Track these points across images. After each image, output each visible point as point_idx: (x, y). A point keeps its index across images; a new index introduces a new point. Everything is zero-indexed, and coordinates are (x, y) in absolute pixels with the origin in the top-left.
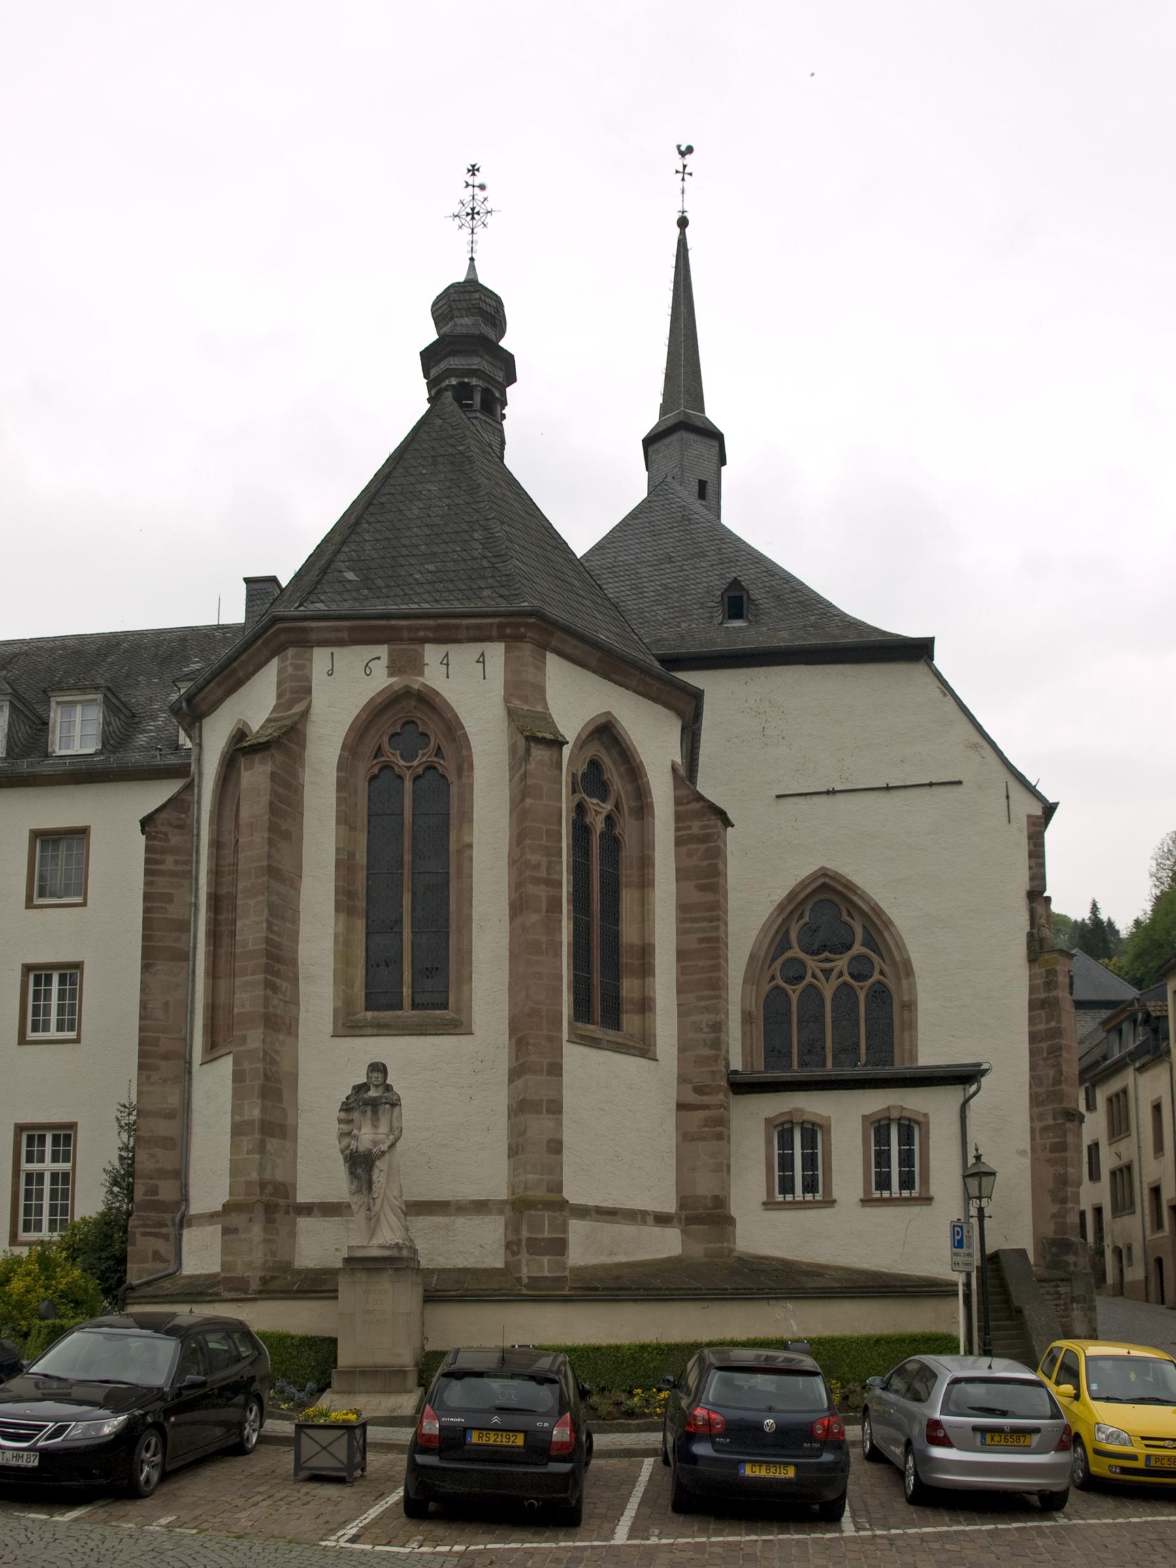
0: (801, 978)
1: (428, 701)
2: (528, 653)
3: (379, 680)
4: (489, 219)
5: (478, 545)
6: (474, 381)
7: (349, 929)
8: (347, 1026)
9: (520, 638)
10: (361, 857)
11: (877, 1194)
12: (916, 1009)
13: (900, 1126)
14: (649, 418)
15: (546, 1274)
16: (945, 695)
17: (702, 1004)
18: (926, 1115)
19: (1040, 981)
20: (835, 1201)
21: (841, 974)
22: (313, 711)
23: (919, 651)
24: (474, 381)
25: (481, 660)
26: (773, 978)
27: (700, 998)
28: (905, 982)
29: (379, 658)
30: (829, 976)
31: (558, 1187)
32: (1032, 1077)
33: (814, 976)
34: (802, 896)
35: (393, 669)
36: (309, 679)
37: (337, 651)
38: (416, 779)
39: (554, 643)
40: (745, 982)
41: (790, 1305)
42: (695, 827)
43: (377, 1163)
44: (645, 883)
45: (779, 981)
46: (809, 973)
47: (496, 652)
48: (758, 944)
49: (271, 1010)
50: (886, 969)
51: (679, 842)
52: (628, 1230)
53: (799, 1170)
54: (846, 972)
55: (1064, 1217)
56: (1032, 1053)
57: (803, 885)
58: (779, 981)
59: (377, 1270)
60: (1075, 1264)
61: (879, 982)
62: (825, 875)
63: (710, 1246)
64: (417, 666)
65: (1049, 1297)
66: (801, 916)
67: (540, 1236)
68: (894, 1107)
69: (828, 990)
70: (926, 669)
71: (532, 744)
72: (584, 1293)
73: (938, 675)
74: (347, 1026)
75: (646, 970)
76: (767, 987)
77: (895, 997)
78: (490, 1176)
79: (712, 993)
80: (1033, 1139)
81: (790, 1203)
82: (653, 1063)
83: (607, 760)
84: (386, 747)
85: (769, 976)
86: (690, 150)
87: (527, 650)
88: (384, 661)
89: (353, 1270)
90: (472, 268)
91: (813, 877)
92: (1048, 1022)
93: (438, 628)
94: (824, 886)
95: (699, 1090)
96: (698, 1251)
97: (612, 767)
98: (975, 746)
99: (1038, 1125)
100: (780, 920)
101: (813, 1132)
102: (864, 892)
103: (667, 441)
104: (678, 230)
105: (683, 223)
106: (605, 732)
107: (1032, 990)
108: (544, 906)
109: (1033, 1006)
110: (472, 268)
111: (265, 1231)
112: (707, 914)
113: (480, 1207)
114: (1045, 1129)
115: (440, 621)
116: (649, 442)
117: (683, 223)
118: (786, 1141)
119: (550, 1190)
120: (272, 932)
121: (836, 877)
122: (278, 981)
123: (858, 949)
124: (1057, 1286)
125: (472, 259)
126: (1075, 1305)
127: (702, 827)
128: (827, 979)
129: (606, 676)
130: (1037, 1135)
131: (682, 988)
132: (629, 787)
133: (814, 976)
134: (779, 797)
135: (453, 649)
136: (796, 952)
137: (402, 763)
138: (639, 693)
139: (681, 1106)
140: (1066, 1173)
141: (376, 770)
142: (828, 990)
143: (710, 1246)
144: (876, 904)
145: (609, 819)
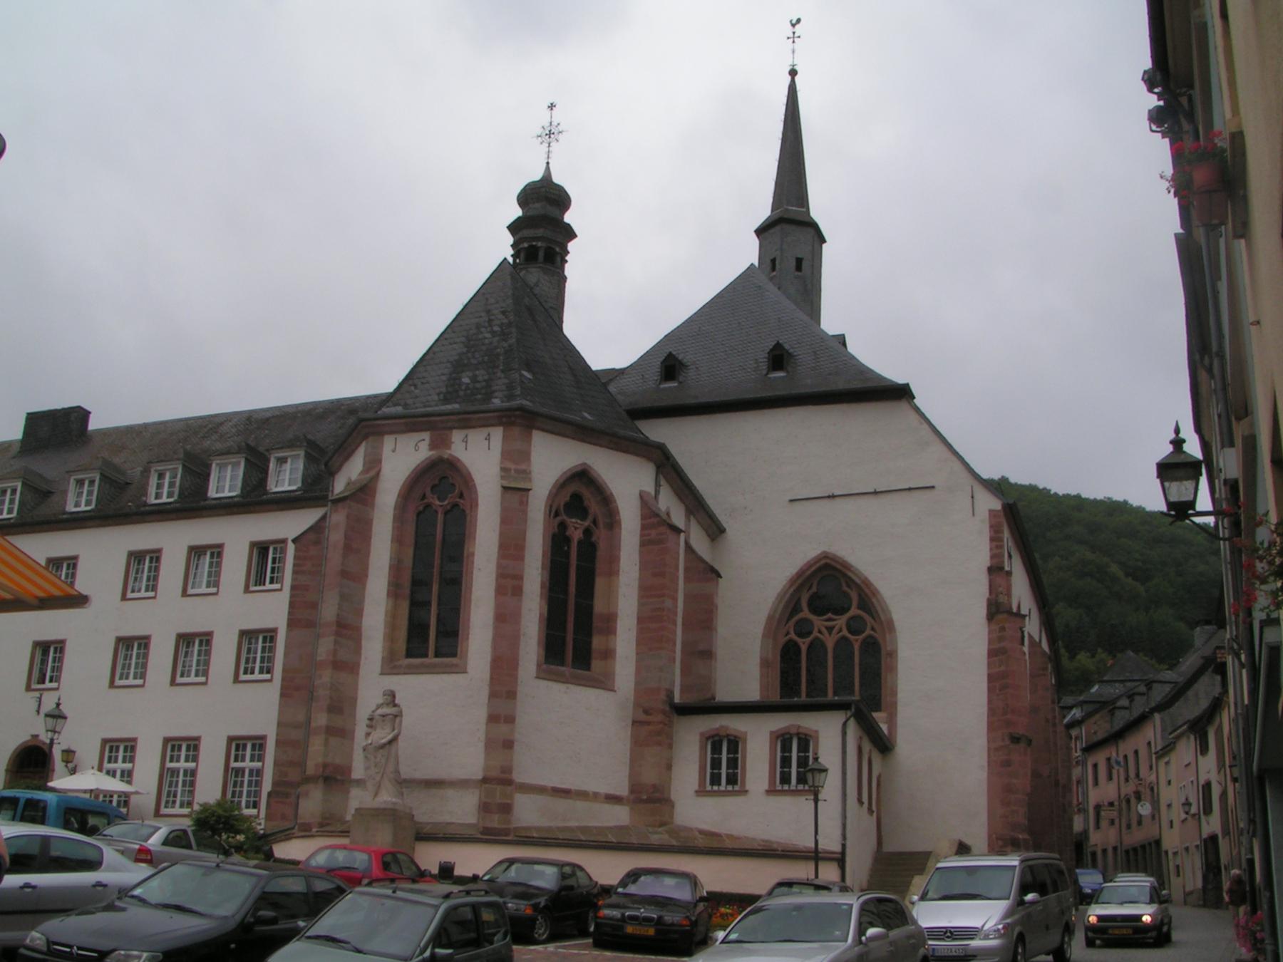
0: (810, 633)
6: (539, 244)
8: (390, 666)
11: (779, 788)
13: (799, 739)
14: (763, 211)
18: (816, 732)
21: (840, 630)
23: (901, 393)
25: (488, 438)
26: (788, 633)
30: (829, 630)
34: (809, 572)
35: (433, 446)
38: (446, 513)
44: (613, 572)
45: (793, 636)
46: (816, 630)
47: (497, 433)
50: (876, 626)
51: (643, 544)
52: (580, 805)
53: (724, 767)
57: (809, 565)
58: (793, 636)
61: (870, 636)
66: (811, 587)
69: (830, 642)
73: (917, 410)
74: (390, 666)
75: (610, 630)
76: (783, 640)
83: (586, 494)
84: (428, 493)
86: (799, 21)
87: (516, 431)
88: (427, 442)
91: (818, 559)
94: (827, 566)
95: (646, 712)
101: (735, 744)
103: (772, 231)
105: (793, 73)
106: (582, 476)
107: (990, 643)
109: (992, 653)
113: (463, 784)
114: (996, 749)
116: (760, 232)
117: (793, 73)
119: (503, 772)
123: (854, 611)
129: (583, 441)
133: (820, 632)
136: (806, 613)
137: (438, 503)
141: (421, 508)
142: (830, 642)
145: (588, 532)
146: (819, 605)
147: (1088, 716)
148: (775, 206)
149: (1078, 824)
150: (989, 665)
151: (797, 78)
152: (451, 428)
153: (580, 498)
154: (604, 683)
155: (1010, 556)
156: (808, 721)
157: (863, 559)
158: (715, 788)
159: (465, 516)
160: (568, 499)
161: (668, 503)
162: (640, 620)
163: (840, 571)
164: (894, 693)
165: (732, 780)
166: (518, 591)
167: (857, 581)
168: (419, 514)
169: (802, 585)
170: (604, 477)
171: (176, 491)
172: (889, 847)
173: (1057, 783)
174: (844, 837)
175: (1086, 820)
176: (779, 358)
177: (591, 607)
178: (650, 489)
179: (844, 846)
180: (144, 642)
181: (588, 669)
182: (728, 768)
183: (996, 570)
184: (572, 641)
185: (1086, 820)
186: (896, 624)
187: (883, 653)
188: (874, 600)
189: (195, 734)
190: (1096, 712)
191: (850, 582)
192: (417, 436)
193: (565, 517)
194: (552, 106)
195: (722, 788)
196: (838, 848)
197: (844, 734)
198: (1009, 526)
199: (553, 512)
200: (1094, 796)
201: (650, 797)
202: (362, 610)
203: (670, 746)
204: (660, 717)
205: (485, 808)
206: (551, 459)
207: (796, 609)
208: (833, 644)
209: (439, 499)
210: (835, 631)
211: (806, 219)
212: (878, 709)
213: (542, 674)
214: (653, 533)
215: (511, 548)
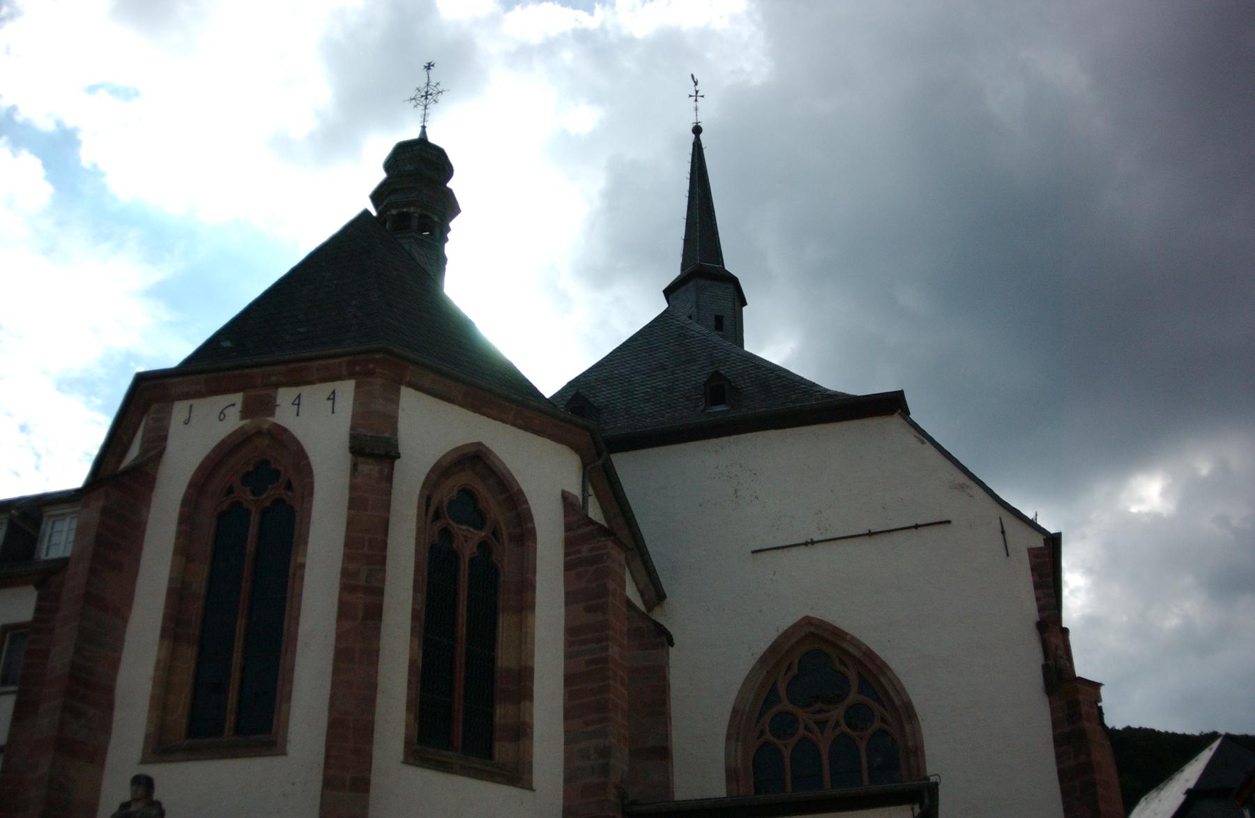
1: (282, 439)
3: (233, 422)
4: (440, 97)
6: (412, 209)
9: (371, 373)
10: (200, 586)
16: (923, 443)
21: (837, 724)
25: (332, 397)
28: (907, 727)
35: (246, 412)
36: (166, 429)
37: (195, 402)
40: (728, 738)
42: (585, 551)
54: (842, 722)
57: (786, 635)
64: (268, 406)
66: (789, 668)
70: (901, 421)
73: (915, 426)
83: (481, 489)
88: (239, 407)
94: (811, 634)
102: (853, 638)
105: (697, 130)
117: (697, 130)
123: (853, 697)
125: (424, 127)
131: (569, 714)
133: (807, 728)
134: (754, 552)
135: (306, 390)
136: (786, 705)
137: (251, 497)
138: (520, 427)
144: (868, 648)
145: (484, 546)
148: (682, 270)
151: (702, 136)
157: (858, 620)
162: (569, 679)
166: (374, 613)
177: (492, 660)
178: (575, 490)
184: (465, 718)
186: (918, 709)
192: (221, 401)
194: (429, 67)
199: (430, 509)
202: (119, 659)
209: (253, 493)
214: (585, 551)
215: (365, 546)
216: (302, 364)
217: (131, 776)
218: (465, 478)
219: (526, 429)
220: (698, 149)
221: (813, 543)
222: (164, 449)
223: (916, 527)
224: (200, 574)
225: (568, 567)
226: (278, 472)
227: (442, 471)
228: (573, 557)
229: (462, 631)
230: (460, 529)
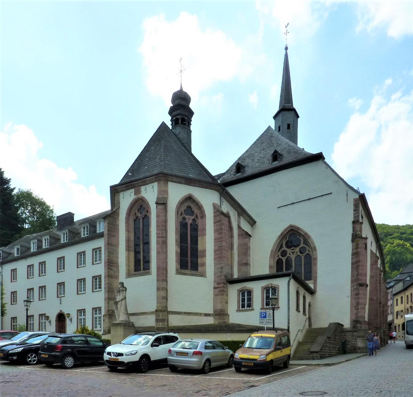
2: (162, 183)
5: (158, 159)
6: (179, 117)
7: (129, 255)
9: (160, 180)
10: (132, 238)
11: (265, 307)
12: (317, 260)
13: (272, 289)
14: (276, 109)
15: (161, 327)
17: (219, 262)
18: (278, 285)
19: (354, 247)
20: (254, 309)
22: (120, 207)
23: (319, 157)
24: (179, 117)
26: (279, 256)
27: (218, 261)
29: (132, 192)
30: (292, 254)
31: (166, 307)
32: (352, 275)
33: (290, 254)
34: (285, 233)
35: (135, 194)
38: (143, 218)
39: (169, 180)
40: (270, 258)
41: (228, 334)
43: (118, 303)
45: (280, 257)
46: (288, 254)
47: (155, 185)
48: (273, 248)
49: (110, 274)
50: (310, 250)
53: (246, 302)
55: (358, 314)
56: (352, 268)
57: (285, 230)
58: (280, 257)
59: (117, 326)
60: (360, 327)
61: (308, 254)
62: (291, 227)
63: (219, 321)
65: (350, 336)
66: (286, 238)
67: (159, 318)
68: (269, 284)
69: (293, 257)
71: (157, 205)
72: (171, 331)
75: (204, 255)
77: (312, 257)
78: (152, 306)
79: (221, 260)
80: (351, 292)
81: (243, 310)
82: (205, 278)
83: (192, 206)
85: (277, 255)
87: (162, 183)
88: (133, 193)
89: (113, 326)
90: (181, 86)
92: (356, 258)
93: (142, 182)
94: (292, 229)
95: (218, 284)
96: (217, 323)
97: (194, 207)
98: (337, 182)
99: (353, 288)
100: (279, 240)
101: (250, 293)
104: (285, 51)
105: (286, 48)
106: (189, 198)
107: (353, 250)
108: (161, 243)
109: (352, 255)
110: (181, 86)
111: (109, 320)
112: (220, 240)
114: (354, 289)
115: (142, 180)
116: (275, 117)
117: (286, 48)
118: (243, 295)
120: (109, 257)
121: (294, 227)
122: (112, 268)
123: (302, 245)
124: (353, 333)
125: (181, 84)
126: (358, 338)
127: (219, 218)
128: (293, 254)
130: (352, 291)
132: (199, 211)
133: (290, 254)
135: (147, 186)
136: (284, 248)
139: (215, 288)
140: (359, 302)
141: (135, 218)
143: (219, 321)
145: (194, 220)
146: (290, 245)
147: (396, 284)
149: (390, 318)
150: (352, 259)
151: (288, 51)
152: (141, 186)
153: (189, 206)
154: (203, 275)
155: (362, 217)
156: (275, 282)
157: (304, 225)
158: (243, 309)
159: (149, 218)
160: (185, 208)
161: (226, 208)
163: (296, 231)
164: (316, 273)
165: (249, 306)
167: (303, 234)
168: (135, 221)
169: (283, 238)
170: (198, 199)
171: (88, 232)
172: (315, 326)
173: (380, 303)
174: (289, 323)
175: (393, 316)
176: (276, 156)
177: (197, 249)
178: (217, 202)
179: (288, 327)
180: (84, 279)
181: (197, 270)
182: (247, 301)
183: (356, 222)
184: (190, 260)
185: (393, 316)
187: (312, 259)
188: (309, 240)
189: (100, 306)
190: (398, 283)
191: (300, 235)
193: (185, 215)
195: (246, 308)
196: (286, 328)
197: (289, 285)
198: (362, 204)
200: (397, 309)
201: (221, 313)
203: (227, 295)
204: (222, 285)
205: (157, 320)
206: (176, 193)
207: (281, 247)
208: (295, 257)
210: (295, 253)
211: (292, 108)
212: (310, 279)
213: (178, 273)
216: (145, 180)
217: (352, 222)
218: (187, 204)
219: (202, 187)
220: (286, 56)
221: (294, 203)
222: (119, 207)
223: (309, 199)
224: (132, 235)
225: (215, 223)
226: (145, 208)
227: (181, 203)
228: (215, 220)
229: (189, 242)
230: (187, 217)
